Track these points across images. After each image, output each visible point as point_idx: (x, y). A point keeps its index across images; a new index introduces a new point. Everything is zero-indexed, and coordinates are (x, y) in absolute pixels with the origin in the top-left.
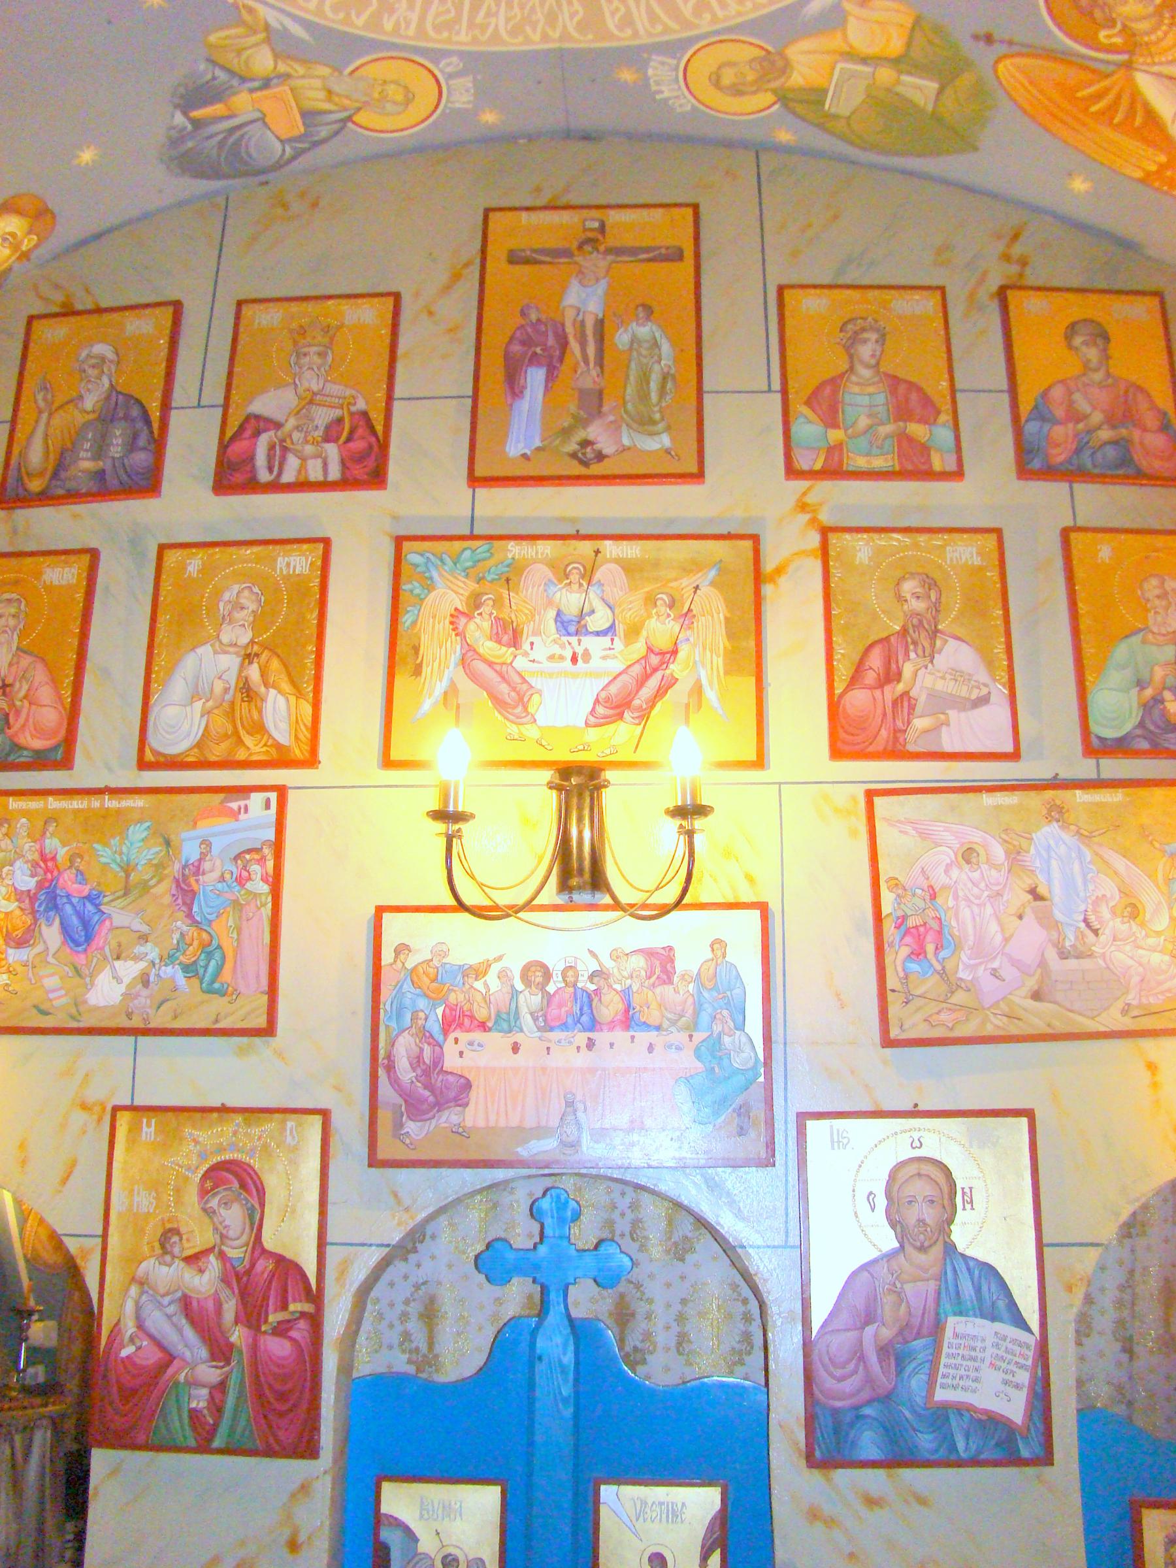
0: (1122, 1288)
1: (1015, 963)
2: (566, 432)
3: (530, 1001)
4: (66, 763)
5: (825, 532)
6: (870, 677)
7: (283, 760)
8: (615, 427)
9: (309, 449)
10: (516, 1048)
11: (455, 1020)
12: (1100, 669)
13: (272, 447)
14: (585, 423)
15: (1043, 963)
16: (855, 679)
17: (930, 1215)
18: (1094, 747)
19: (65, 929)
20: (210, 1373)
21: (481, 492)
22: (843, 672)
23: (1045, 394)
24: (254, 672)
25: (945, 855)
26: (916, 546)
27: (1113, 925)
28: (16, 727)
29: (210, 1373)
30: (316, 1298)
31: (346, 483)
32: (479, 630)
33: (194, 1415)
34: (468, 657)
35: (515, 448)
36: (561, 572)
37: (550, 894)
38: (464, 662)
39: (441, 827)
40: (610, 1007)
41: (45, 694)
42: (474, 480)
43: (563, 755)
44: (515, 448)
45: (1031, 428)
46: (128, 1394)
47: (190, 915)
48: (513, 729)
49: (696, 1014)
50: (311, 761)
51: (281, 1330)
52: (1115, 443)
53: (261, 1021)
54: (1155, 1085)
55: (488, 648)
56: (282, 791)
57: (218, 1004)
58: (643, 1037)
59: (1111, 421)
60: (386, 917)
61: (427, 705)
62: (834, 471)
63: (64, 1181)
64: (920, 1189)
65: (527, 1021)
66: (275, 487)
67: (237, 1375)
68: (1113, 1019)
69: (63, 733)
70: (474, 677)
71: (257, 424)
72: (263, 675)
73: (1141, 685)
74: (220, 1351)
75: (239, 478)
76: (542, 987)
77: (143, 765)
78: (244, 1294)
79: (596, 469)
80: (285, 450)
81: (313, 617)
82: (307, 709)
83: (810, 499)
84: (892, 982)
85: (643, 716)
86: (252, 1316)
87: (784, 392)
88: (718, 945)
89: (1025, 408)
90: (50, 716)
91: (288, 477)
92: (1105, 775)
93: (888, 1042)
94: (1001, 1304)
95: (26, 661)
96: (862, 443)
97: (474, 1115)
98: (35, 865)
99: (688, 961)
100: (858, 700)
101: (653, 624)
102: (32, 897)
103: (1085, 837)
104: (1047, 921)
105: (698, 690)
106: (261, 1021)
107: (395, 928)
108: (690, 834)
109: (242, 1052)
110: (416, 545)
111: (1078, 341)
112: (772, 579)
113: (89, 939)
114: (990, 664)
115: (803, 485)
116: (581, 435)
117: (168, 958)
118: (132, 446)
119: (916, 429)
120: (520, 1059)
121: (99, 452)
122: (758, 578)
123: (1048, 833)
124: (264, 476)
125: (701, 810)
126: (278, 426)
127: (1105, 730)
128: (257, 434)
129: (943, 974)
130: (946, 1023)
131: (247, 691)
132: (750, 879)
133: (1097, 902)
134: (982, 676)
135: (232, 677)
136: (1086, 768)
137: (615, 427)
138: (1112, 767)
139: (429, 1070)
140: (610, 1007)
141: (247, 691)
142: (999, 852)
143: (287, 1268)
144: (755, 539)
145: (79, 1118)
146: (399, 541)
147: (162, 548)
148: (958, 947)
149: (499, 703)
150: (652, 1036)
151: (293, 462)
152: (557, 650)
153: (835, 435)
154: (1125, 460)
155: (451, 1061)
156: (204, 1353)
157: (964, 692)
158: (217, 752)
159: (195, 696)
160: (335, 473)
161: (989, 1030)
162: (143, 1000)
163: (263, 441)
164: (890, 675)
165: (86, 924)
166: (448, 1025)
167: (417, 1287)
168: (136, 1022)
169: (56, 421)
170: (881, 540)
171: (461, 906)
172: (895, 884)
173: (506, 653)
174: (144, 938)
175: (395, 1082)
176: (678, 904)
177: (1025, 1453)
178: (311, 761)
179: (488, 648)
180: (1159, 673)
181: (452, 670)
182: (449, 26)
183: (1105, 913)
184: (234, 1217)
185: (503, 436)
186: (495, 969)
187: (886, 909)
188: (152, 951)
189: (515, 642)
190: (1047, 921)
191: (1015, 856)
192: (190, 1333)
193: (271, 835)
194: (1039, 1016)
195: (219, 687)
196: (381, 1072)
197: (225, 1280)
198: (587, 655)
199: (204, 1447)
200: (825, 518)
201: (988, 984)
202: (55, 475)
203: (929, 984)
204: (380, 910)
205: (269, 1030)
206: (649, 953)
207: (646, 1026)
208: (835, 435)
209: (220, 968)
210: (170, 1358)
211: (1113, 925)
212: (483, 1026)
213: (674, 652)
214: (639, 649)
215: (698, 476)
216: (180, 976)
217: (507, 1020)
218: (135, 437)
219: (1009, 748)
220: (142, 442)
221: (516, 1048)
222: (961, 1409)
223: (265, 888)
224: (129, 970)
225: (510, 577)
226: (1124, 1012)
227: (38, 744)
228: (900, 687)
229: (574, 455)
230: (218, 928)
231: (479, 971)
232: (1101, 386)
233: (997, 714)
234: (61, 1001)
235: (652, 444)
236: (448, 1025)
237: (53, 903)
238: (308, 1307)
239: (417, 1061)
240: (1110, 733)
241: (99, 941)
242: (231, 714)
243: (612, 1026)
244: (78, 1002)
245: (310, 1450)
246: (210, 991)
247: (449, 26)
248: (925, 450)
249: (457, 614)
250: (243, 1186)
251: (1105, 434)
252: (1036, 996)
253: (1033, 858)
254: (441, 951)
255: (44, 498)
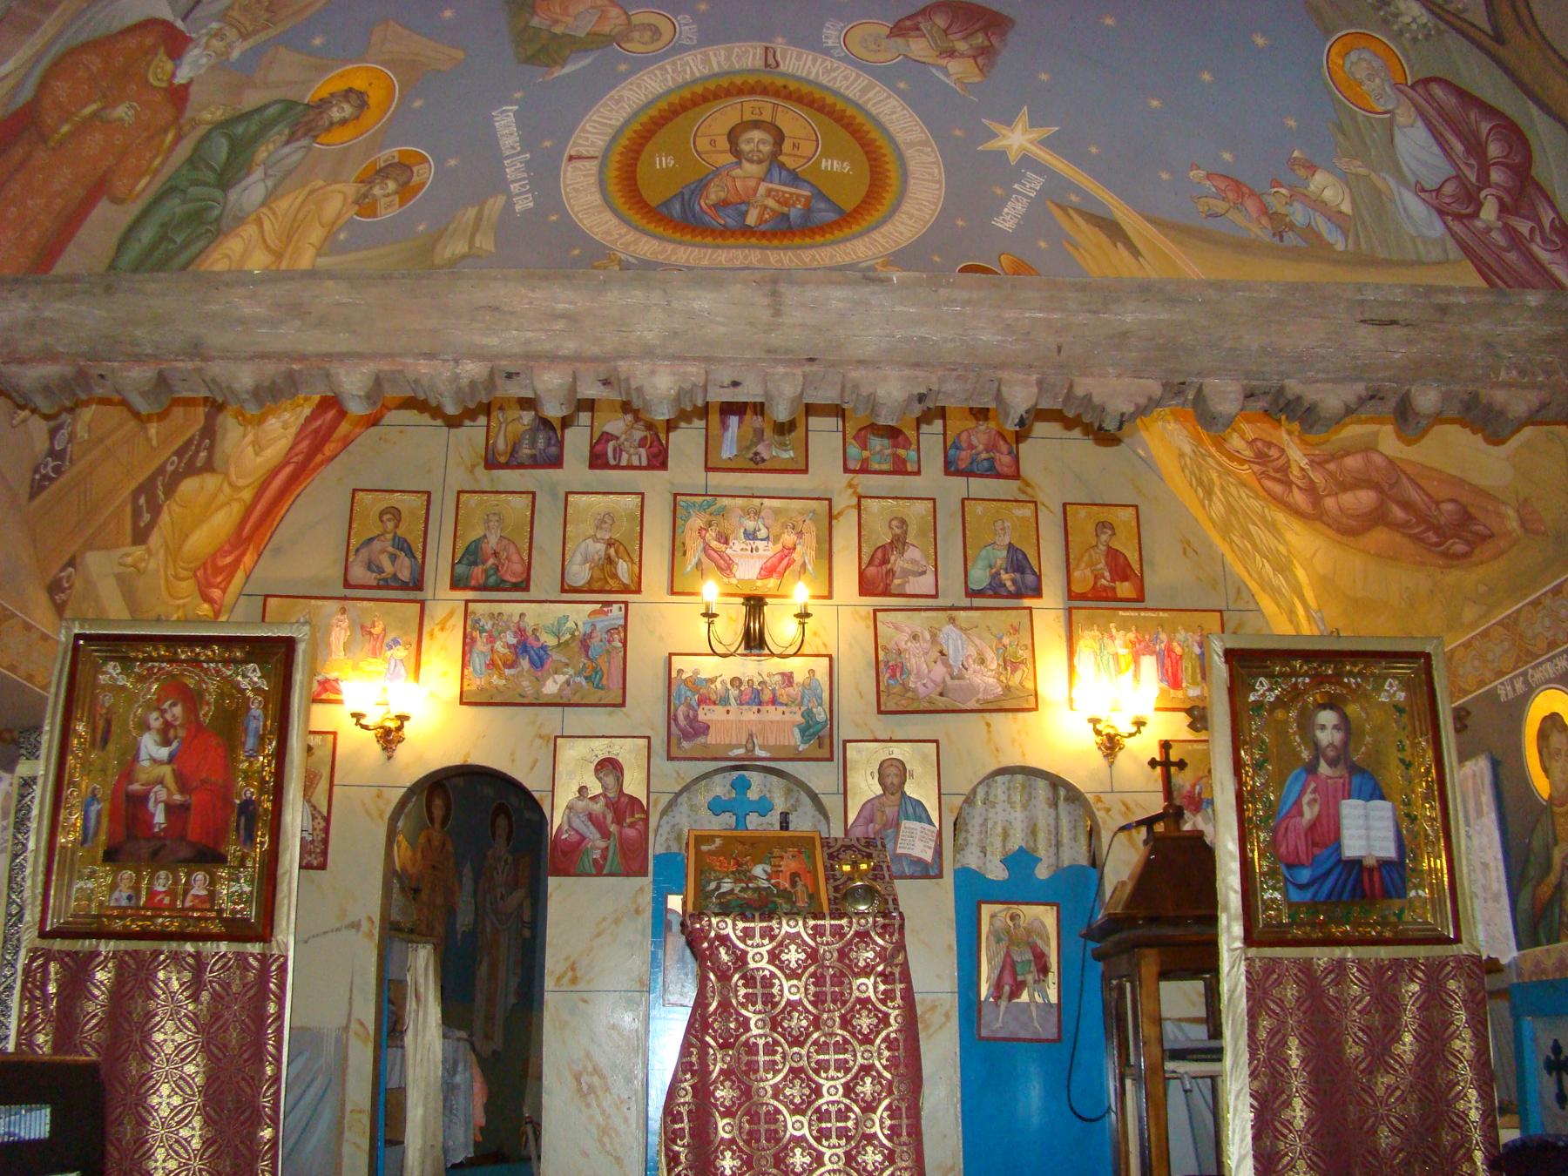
0: (982, 825)
1: (933, 681)
2: (748, 448)
3: (734, 692)
4: (527, 589)
5: (860, 498)
6: (877, 561)
7: (626, 590)
8: (769, 446)
9: (632, 450)
10: (728, 712)
11: (703, 700)
12: (975, 561)
13: (615, 450)
14: (756, 444)
15: (944, 681)
16: (870, 563)
17: (896, 781)
18: (971, 593)
19: (532, 662)
20: (602, 844)
21: (710, 474)
22: (866, 559)
23: (959, 436)
24: (612, 551)
25: (905, 637)
26: (898, 505)
27: (974, 666)
28: (503, 572)
29: (602, 844)
30: (647, 813)
31: (650, 467)
32: (711, 535)
33: (595, 861)
34: (706, 549)
35: (725, 455)
36: (747, 512)
37: (742, 650)
38: (705, 550)
39: (706, 619)
40: (767, 696)
41: (515, 558)
42: (708, 469)
43: (748, 592)
44: (725, 455)
45: (952, 452)
46: (564, 853)
47: (587, 656)
48: (726, 580)
49: (803, 698)
50: (639, 591)
51: (632, 825)
52: (987, 459)
53: (619, 700)
54: (989, 732)
55: (714, 544)
56: (626, 603)
57: (600, 693)
58: (781, 709)
59: (987, 450)
60: (673, 658)
61: (689, 569)
62: (865, 470)
63: (532, 768)
64: (893, 771)
65: (732, 700)
66: (618, 467)
67: (612, 843)
68: (972, 705)
69: (525, 576)
70: (708, 556)
71: (606, 437)
72: (616, 552)
73: (991, 567)
74: (605, 834)
75: (599, 462)
76: (739, 687)
77: (563, 591)
78: (615, 812)
79: (762, 466)
80: (621, 450)
81: (638, 529)
82: (636, 569)
83: (854, 482)
84: (882, 688)
85: (782, 575)
86: (619, 820)
87: (844, 432)
88: (812, 671)
89: (949, 444)
90: (518, 568)
91: (624, 463)
92: (974, 605)
93: (880, 712)
94: (924, 816)
95: (505, 542)
96: (878, 457)
97: (712, 739)
98: (515, 633)
99: (799, 678)
100: (872, 570)
101: (785, 536)
102: (515, 647)
103: (963, 630)
104: (946, 664)
105: (804, 565)
106: (619, 700)
107: (677, 662)
108: (803, 624)
109: (610, 714)
110: (684, 498)
111: (386, 517)
112: (836, 518)
113: (542, 666)
114: (926, 556)
115: (851, 475)
116: (754, 450)
117: (579, 674)
118: (548, 444)
119: (901, 452)
120: (730, 717)
121: (533, 444)
122: (831, 517)
123: (949, 628)
124: (612, 462)
125: (808, 615)
126: (617, 438)
127: (974, 586)
128: (608, 441)
129: (903, 685)
130: (904, 704)
131: (609, 560)
132: (825, 645)
133: (967, 657)
134: (924, 563)
135: (602, 554)
136: (966, 602)
137: (769, 446)
138: (977, 602)
139: (692, 720)
140: (767, 696)
141: (609, 560)
142: (928, 636)
143: (633, 801)
144: (830, 500)
145: (539, 742)
146: (675, 495)
147: (567, 494)
148: (910, 674)
149: (720, 568)
150: (784, 708)
151: (625, 456)
152: (744, 546)
153: (866, 454)
154: (992, 468)
155: (701, 717)
156: (598, 836)
157: (916, 569)
158: (596, 586)
159: (585, 561)
160: (644, 463)
161: (921, 708)
162: (568, 691)
163: (610, 446)
164: (885, 561)
165: (540, 658)
166: (700, 702)
167: (673, 826)
168: (564, 701)
169: (510, 428)
170: (883, 503)
171: (715, 653)
172: (884, 648)
173: (723, 547)
174: (567, 665)
175: (677, 725)
176: (795, 655)
177: (932, 873)
178: (639, 591)
179: (714, 544)
180: (999, 562)
181: (699, 554)
182: (700, 259)
183: (971, 661)
184: (610, 780)
185: (720, 447)
186: (719, 680)
187: (880, 658)
188: (571, 671)
189: (726, 542)
190: (946, 664)
191: (934, 637)
192: (592, 828)
193: (622, 622)
194: (942, 703)
195: (596, 557)
196: (672, 722)
197: (607, 805)
198: (757, 549)
199: (599, 874)
200: (860, 491)
201: (921, 690)
202: (512, 455)
203: (898, 689)
204: (671, 655)
205: (623, 704)
206: (783, 674)
207: (781, 704)
208: (866, 454)
209: (601, 679)
210: (583, 838)
211: (974, 666)
212: (715, 703)
213: (794, 549)
214: (779, 546)
215: (805, 471)
216: (584, 682)
217: (724, 701)
218: (550, 439)
219: (933, 593)
220: (553, 442)
221: (728, 712)
222: (907, 856)
223: (620, 645)
224: (561, 679)
225: (723, 512)
226: (978, 701)
227: (514, 580)
228: (889, 566)
229: (751, 459)
230: (599, 661)
231: (712, 681)
232: (984, 433)
233: (929, 579)
234: (530, 691)
235: (785, 455)
236: (700, 702)
237: (525, 651)
238: (643, 816)
239: (687, 717)
240: (976, 588)
241: (546, 666)
242: (602, 570)
243: (767, 704)
244: (538, 692)
245: (645, 874)
246: (597, 687)
247: (700, 259)
248: (904, 462)
249: (701, 529)
250: (614, 768)
251: (984, 455)
252: (941, 694)
253: (941, 637)
254: (696, 672)
255: (506, 466)
